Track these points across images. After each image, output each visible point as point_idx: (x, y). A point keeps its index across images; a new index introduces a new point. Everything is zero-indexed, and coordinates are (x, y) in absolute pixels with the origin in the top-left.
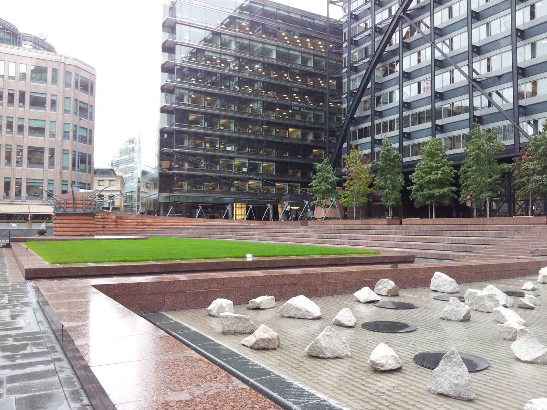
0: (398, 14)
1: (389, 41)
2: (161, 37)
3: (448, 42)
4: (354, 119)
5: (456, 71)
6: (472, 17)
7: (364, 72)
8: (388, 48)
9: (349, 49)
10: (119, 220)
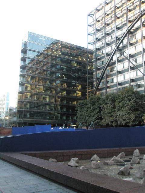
0: (115, 48)
1: (112, 59)
2: (20, 55)
3: (135, 60)
4: (98, 89)
5: (138, 71)
6: (143, 38)
7: (102, 70)
8: (112, 62)
9: (96, 61)
10: (2, 130)
